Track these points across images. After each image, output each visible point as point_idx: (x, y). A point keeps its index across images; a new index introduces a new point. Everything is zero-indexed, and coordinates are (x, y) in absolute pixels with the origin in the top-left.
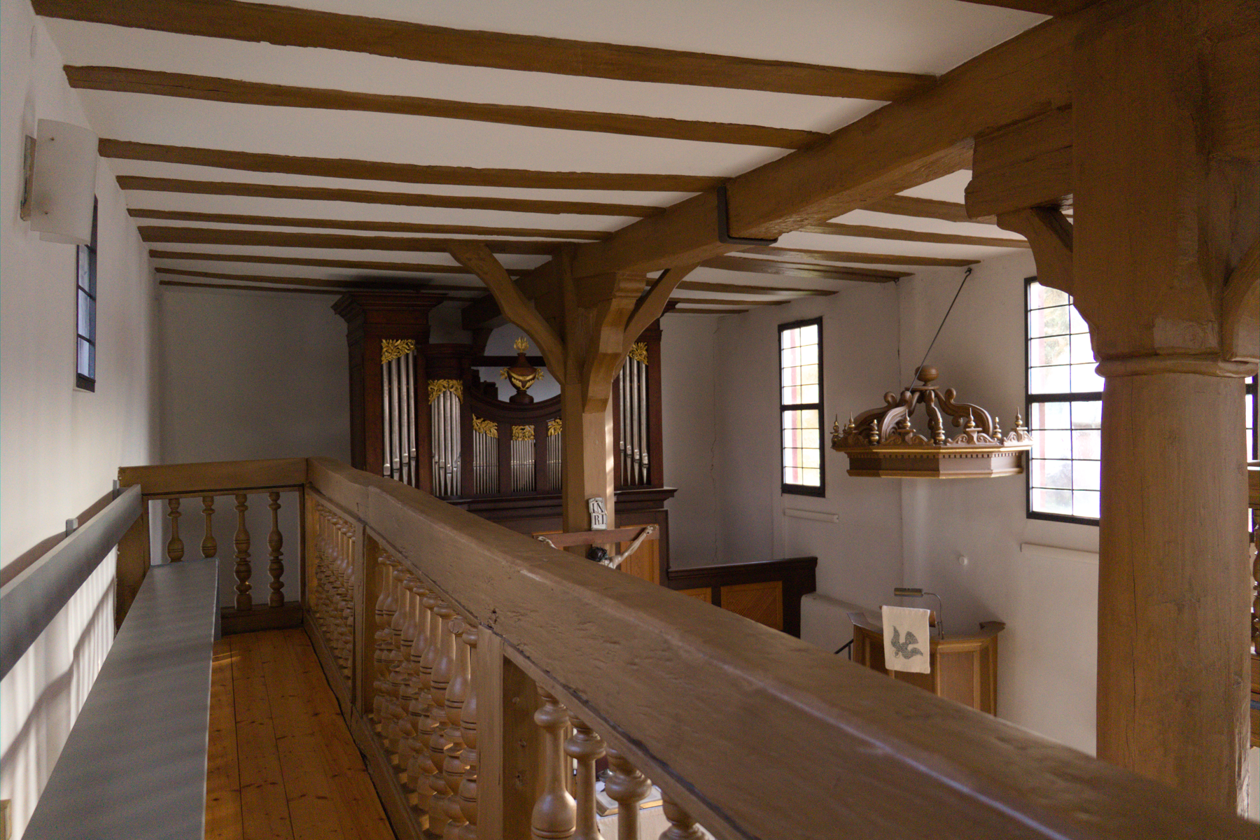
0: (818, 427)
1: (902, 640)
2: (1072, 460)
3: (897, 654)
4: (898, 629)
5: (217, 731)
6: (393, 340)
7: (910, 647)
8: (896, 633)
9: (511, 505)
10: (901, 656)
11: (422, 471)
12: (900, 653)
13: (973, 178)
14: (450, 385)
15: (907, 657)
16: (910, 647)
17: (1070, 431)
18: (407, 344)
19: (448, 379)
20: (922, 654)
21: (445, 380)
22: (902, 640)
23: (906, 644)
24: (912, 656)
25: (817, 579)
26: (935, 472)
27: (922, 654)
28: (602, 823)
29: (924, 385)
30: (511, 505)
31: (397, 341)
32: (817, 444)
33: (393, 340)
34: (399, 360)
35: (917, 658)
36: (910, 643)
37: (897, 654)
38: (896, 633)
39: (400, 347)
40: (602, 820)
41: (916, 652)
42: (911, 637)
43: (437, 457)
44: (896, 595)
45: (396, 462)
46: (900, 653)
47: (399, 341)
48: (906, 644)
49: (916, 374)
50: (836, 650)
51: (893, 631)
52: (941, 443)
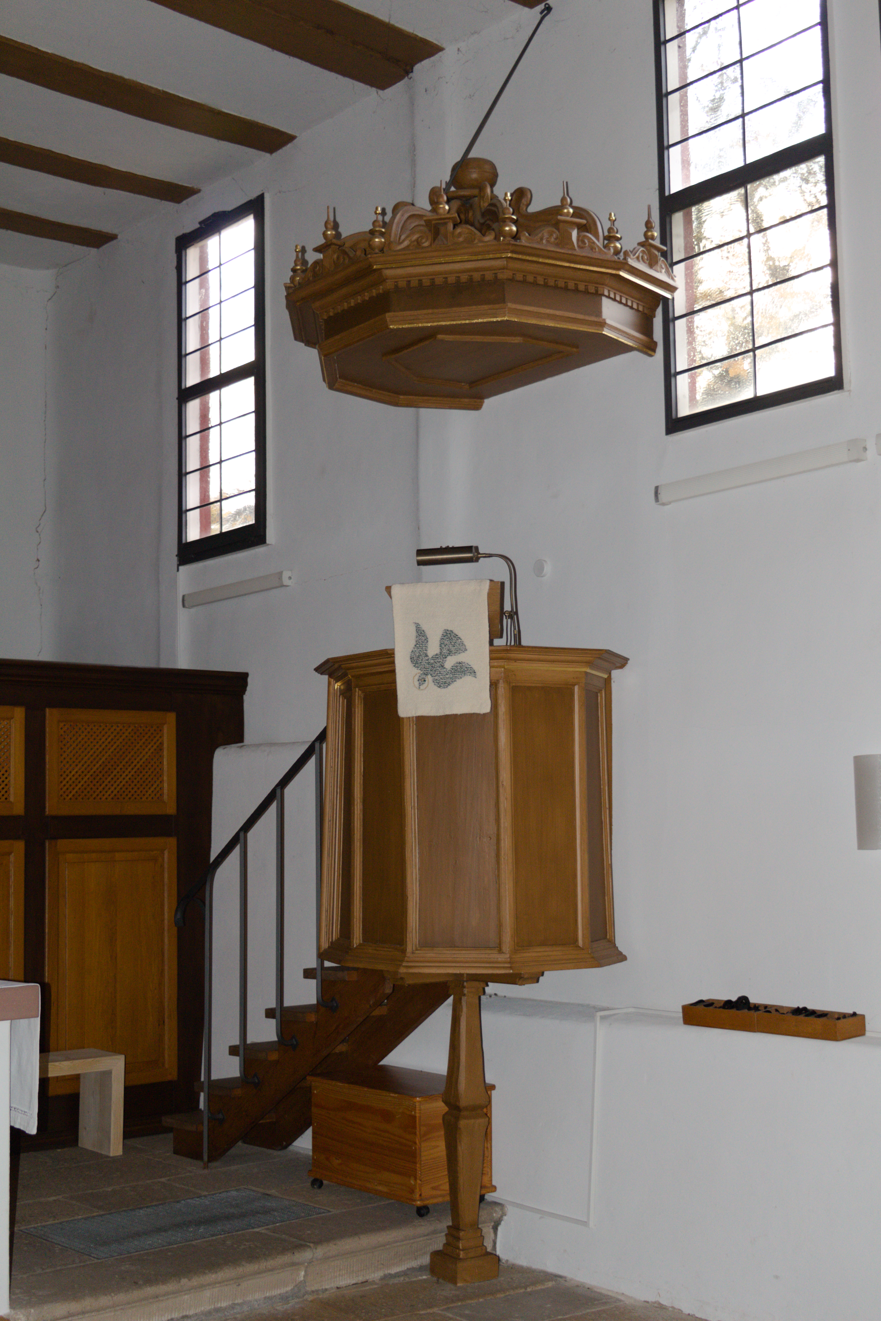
1: (433, 649)
3: (422, 681)
4: (424, 627)
5: (177, 212)
7: (450, 662)
8: (421, 635)
9: (417, 964)
10: (431, 684)
12: (429, 678)
15: (443, 684)
16: (450, 662)
20: (473, 673)
22: (433, 649)
23: (442, 656)
24: (453, 680)
26: (650, 352)
27: (473, 673)
29: (411, 239)
30: (417, 964)
35: (464, 684)
36: (450, 653)
37: (422, 681)
38: (421, 635)
41: (462, 670)
42: (451, 640)
44: (420, 563)
46: (429, 678)
48: (442, 656)
49: (324, 380)
50: (336, 210)
51: (414, 634)
52: (14, 1316)
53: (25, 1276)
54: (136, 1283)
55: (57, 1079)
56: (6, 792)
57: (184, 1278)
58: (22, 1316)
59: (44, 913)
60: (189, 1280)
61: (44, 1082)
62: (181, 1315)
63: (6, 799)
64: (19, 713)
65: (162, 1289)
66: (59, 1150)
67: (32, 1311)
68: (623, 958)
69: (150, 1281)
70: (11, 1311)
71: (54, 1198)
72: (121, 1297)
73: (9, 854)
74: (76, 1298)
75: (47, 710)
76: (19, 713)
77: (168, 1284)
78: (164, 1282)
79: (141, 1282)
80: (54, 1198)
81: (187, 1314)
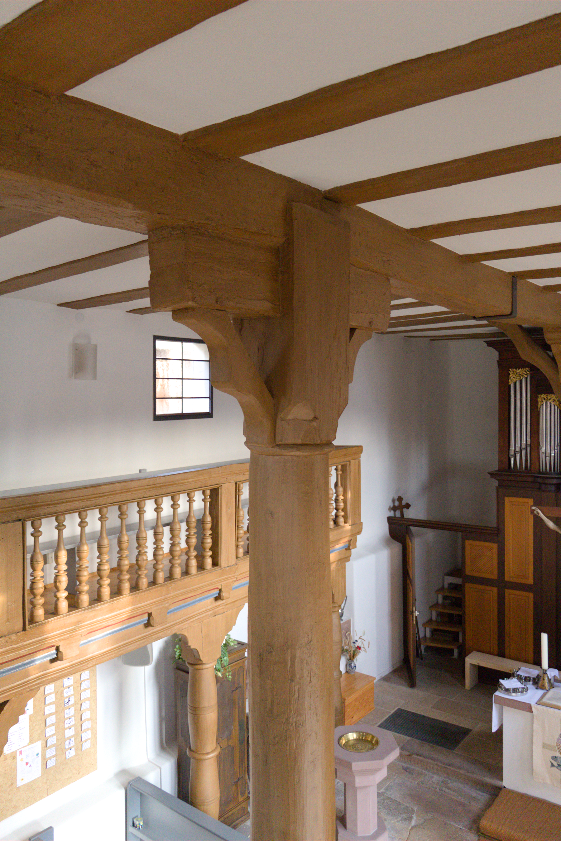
0: (185, 412)
2: (182, 379)
6: (516, 369)
11: (533, 454)
13: (186, 136)
14: (549, 398)
17: (183, 380)
18: (525, 371)
19: (547, 394)
21: (545, 394)
25: (501, 658)
28: (535, 707)
31: (519, 369)
32: (186, 411)
33: (516, 369)
34: (521, 381)
39: (520, 373)
40: (535, 706)
43: (544, 449)
45: (518, 447)
47: (520, 369)
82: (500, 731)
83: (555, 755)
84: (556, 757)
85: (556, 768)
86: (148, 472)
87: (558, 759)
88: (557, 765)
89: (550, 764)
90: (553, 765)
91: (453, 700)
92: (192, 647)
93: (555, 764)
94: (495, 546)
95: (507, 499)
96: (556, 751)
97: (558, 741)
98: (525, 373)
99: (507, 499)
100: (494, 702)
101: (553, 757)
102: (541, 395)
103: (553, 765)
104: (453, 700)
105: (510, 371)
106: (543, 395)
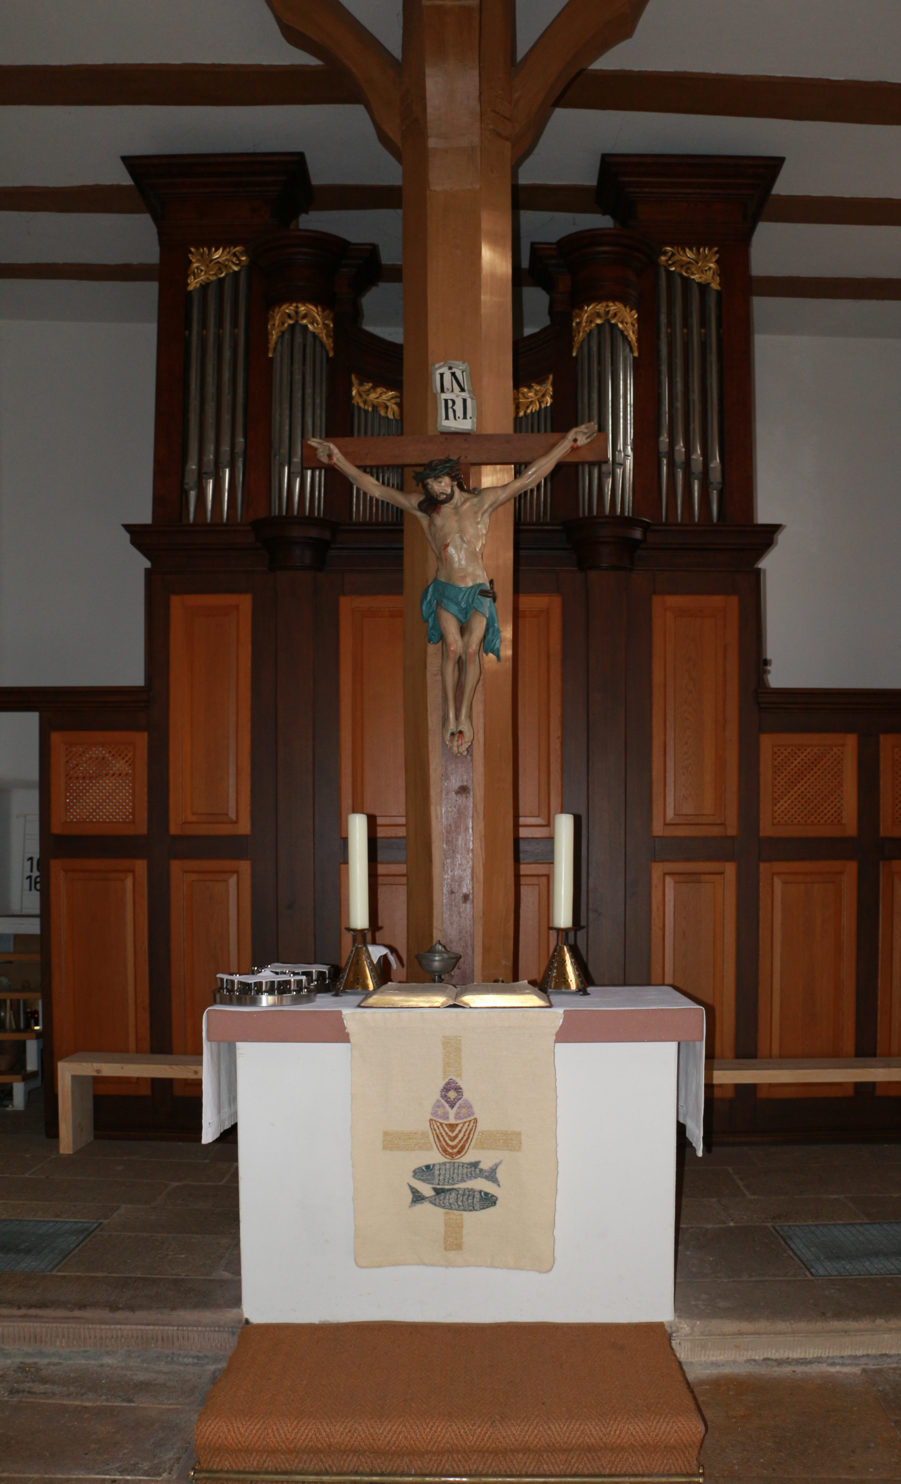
47: (221, 251)
53: (726, 1280)
54: (824, 1314)
55: (721, 1086)
56: (839, 815)
57: (881, 1318)
58: (685, 1326)
59: (878, 929)
60: (886, 1322)
61: (709, 1087)
62: (879, 1353)
63: (839, 821)
64: (851, 741)
65: (852, 1325)
66: (886, 1146)
67: (698, 1323)
68: (128, 527)
69: (840, 1314)
70: (675, 1319)
71: (835, 1196)
72: (802, 1325)
73: (841, 873)
74: (750, 1318)
75: (882, 737)
76: (851, 741)
77: (860, 1322)
78: (855, 1319)
79: (829, 1315)
80: (835, 1196)
81: (888, 1352)
82: (229, 1136)
83: (423, 1163)
84: (428, 1167)
85: (431, 1202)
86: (62, 1154)
87: (437, 1172)
88: (433, 1193)
89: (410, 1196)
90: (417, 1197)
91: (27, 1175)
92: (687, 1135)
93: (426, 1190)
94: (141, 739)
95: (176, 601)
96: (430, 1149)
97: (434, 1113)
98: (234, 260)
99: (176, 601)
100: (209, 1039)
101: (420, 1168)
102: (280, 307)
103: (417, 1197)
104: (27, 1175)
105: (191, 252)
106: (284, 306)
